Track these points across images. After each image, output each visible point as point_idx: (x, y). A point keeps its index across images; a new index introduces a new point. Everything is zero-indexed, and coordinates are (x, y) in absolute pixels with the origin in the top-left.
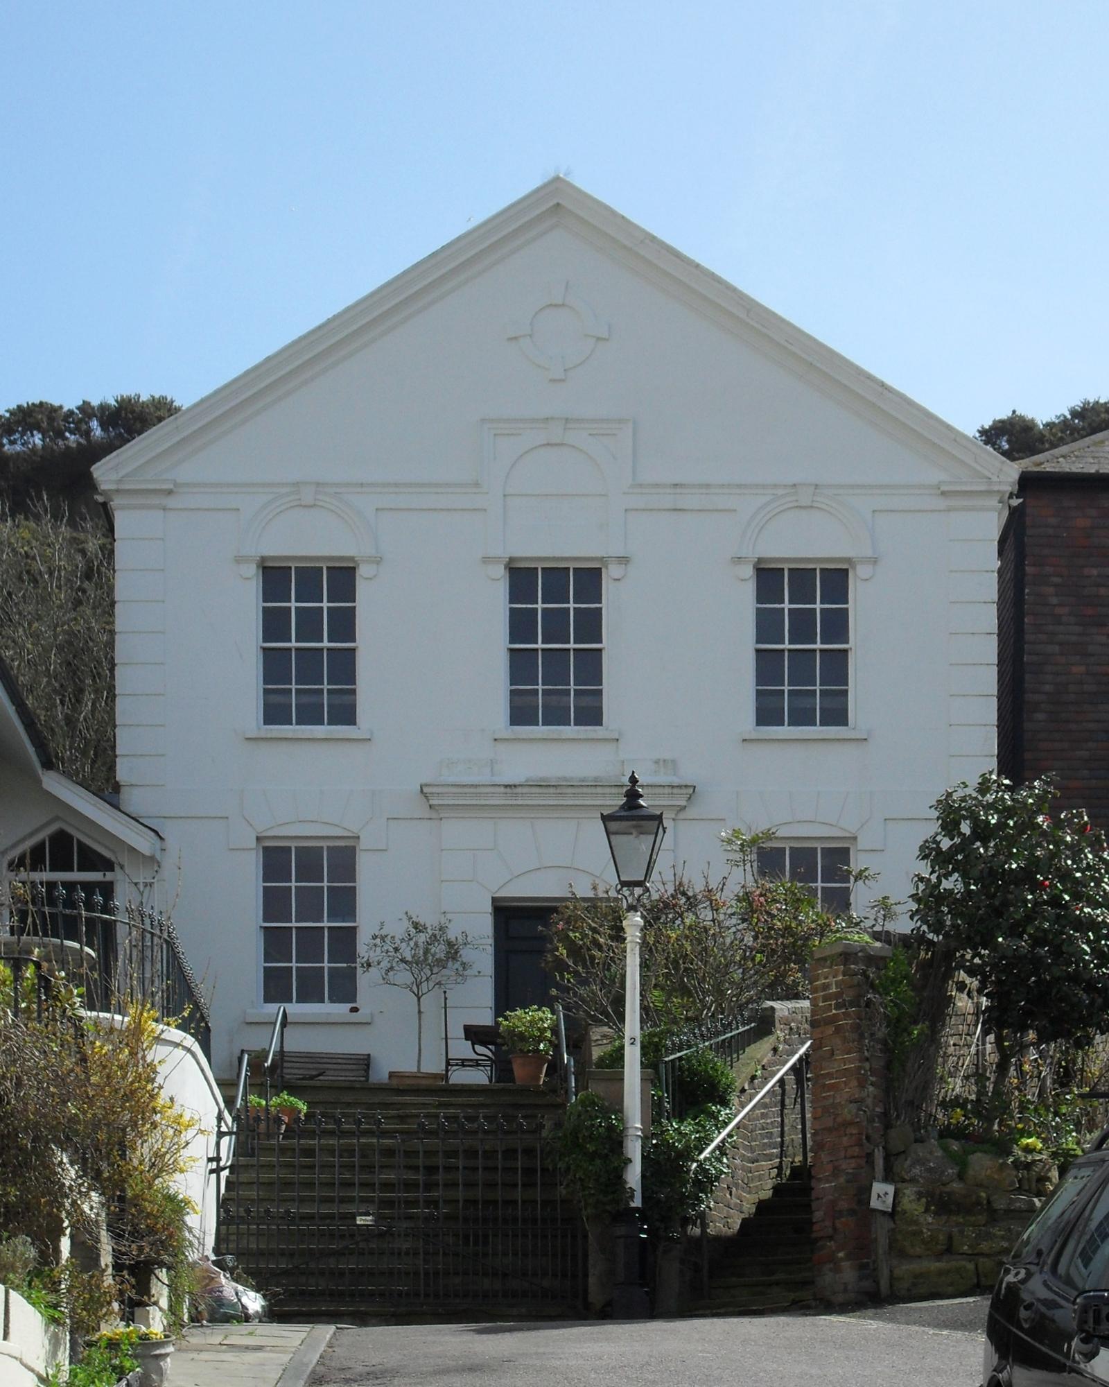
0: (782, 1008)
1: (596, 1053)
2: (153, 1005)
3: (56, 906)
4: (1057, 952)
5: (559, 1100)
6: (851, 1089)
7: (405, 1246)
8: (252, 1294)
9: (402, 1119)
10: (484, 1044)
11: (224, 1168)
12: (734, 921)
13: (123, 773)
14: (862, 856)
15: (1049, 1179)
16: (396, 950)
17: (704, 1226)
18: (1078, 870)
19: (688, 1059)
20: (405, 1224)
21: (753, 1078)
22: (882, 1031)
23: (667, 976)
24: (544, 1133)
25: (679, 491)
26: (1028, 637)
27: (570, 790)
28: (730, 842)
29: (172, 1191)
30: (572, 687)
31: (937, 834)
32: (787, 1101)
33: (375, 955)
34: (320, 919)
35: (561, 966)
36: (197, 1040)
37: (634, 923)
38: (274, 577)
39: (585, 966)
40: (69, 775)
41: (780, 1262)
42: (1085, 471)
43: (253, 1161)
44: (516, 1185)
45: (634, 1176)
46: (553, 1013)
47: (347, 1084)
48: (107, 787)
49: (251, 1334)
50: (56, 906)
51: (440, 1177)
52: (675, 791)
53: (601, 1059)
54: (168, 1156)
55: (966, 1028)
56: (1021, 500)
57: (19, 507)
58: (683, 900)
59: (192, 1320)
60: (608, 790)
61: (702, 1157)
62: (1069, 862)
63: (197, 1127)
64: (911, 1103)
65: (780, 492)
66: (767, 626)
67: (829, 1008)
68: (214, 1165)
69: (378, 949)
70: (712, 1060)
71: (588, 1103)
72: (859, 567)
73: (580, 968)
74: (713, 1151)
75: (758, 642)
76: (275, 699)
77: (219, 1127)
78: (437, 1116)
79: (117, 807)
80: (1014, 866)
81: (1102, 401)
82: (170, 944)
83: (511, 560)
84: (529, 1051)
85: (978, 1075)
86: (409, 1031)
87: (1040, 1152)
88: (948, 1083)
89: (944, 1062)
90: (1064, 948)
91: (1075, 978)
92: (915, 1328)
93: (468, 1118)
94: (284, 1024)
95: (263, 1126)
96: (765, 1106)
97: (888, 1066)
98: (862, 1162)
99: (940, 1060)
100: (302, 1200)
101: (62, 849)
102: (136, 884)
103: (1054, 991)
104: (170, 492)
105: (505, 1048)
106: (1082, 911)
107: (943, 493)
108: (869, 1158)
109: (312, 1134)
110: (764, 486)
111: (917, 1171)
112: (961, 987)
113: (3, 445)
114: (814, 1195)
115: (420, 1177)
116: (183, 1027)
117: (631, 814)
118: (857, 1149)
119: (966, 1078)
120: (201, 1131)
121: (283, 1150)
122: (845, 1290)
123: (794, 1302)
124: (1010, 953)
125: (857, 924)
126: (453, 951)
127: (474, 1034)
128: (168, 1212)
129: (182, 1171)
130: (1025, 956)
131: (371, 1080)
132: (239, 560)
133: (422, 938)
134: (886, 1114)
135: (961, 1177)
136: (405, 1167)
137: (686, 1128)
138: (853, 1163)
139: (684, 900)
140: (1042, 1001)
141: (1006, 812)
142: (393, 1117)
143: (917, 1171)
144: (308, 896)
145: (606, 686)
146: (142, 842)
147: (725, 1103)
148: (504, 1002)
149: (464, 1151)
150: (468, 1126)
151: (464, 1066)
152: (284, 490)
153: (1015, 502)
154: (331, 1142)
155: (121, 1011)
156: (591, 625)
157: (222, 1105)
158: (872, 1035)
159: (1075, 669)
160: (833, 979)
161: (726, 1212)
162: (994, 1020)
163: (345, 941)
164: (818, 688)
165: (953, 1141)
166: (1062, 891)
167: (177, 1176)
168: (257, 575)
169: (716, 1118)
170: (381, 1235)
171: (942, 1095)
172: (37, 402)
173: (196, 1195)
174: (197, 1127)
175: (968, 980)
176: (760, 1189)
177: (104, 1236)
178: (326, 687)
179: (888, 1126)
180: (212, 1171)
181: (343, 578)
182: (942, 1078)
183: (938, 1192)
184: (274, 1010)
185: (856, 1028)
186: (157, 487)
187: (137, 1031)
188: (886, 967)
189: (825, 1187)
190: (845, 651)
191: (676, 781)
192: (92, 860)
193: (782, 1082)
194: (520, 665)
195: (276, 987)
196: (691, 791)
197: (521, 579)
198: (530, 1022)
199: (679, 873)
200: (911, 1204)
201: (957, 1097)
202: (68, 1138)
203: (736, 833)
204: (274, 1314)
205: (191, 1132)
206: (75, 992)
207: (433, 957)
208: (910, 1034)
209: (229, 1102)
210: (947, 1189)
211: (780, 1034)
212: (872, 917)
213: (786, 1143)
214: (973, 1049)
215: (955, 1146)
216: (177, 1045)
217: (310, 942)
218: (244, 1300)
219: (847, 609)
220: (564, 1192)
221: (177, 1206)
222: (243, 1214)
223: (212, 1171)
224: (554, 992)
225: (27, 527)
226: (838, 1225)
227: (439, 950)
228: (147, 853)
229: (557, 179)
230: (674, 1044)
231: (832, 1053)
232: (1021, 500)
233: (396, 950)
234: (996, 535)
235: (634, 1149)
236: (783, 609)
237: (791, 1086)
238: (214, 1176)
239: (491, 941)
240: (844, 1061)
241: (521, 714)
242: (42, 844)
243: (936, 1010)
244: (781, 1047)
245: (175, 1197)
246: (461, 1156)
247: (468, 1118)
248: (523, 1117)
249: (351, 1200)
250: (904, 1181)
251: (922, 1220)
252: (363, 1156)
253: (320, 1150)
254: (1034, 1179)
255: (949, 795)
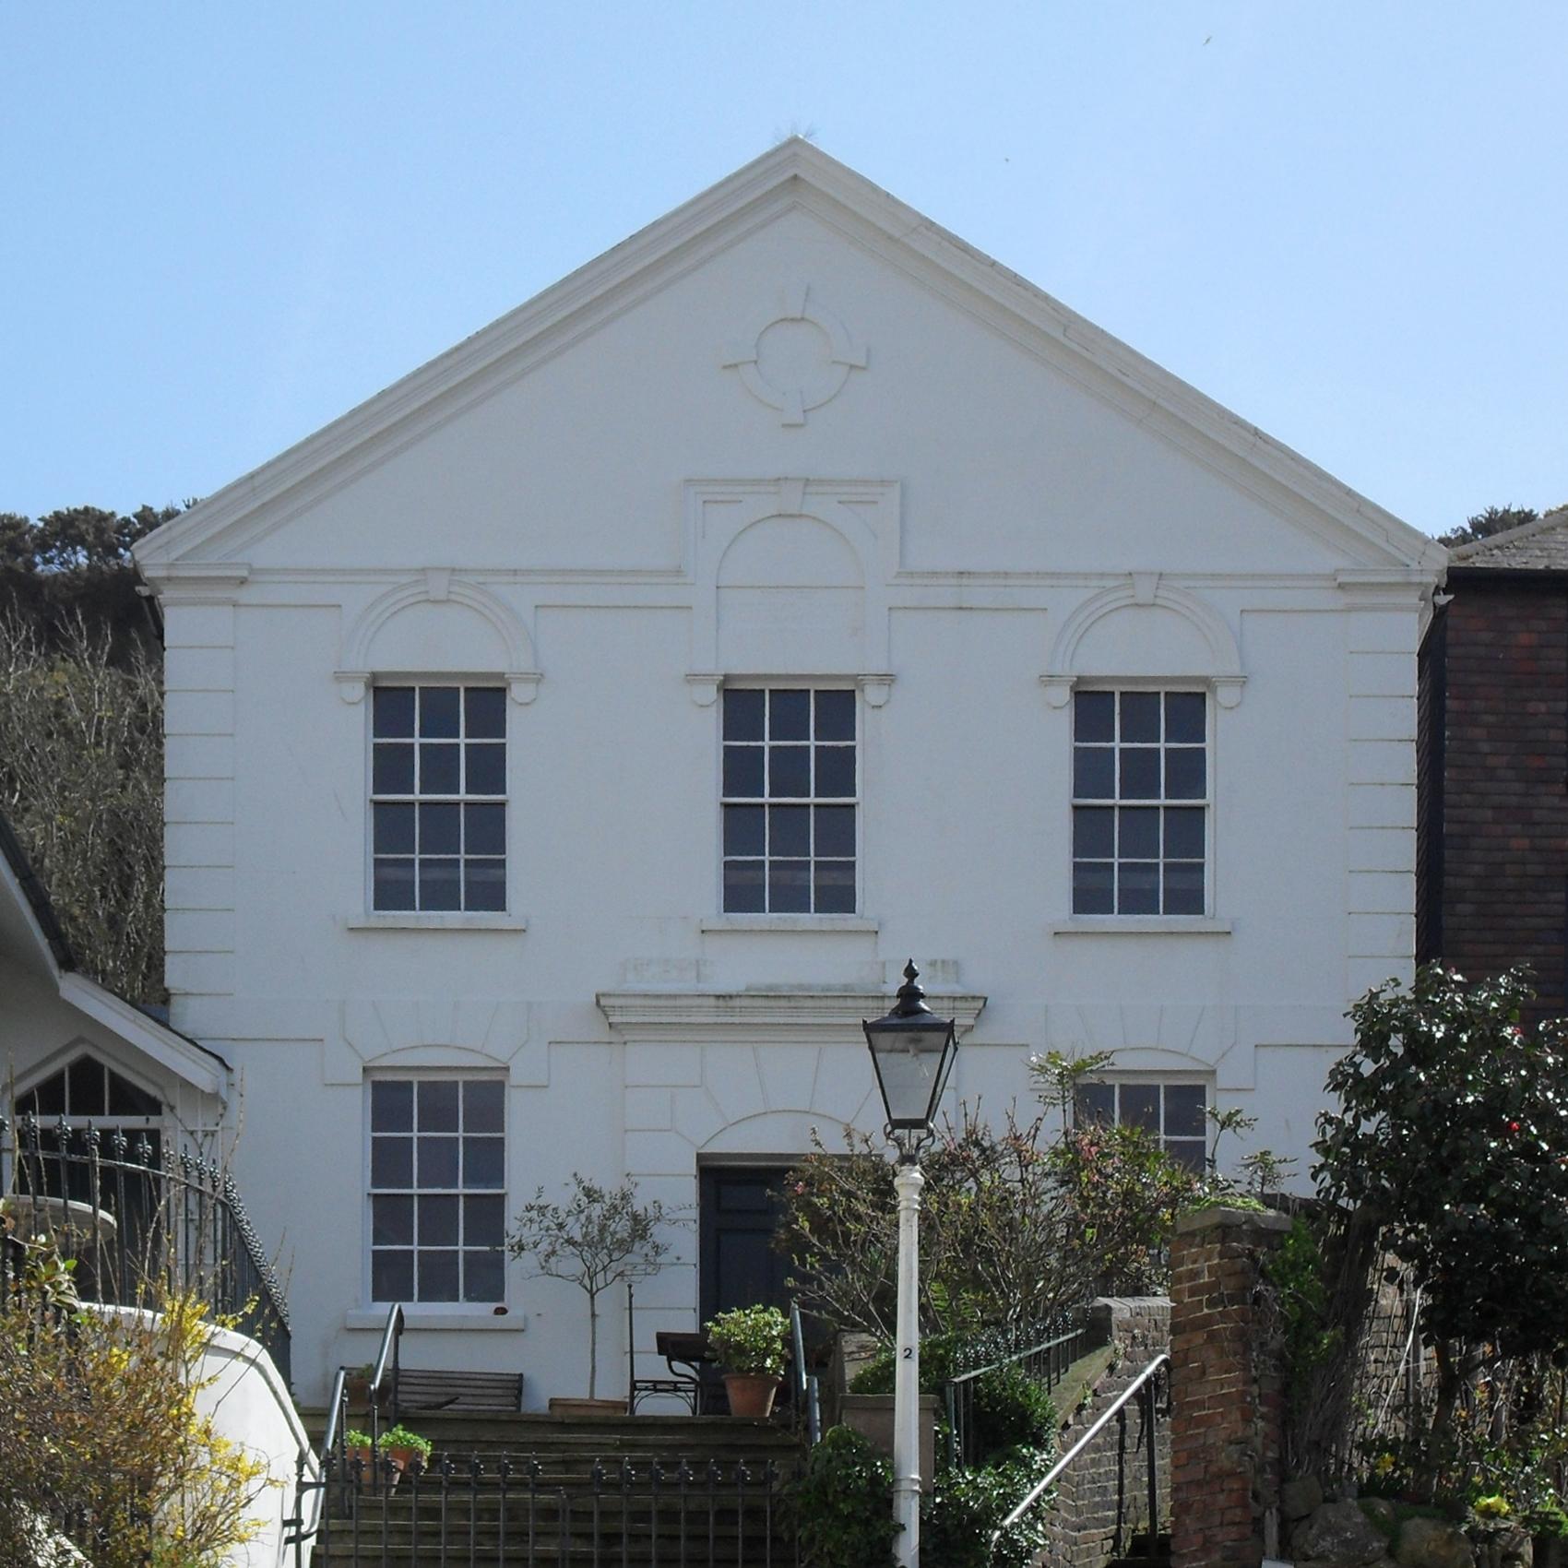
0: (1121, 1307)
1: (851, 1372)
2: (201, 1297)
3: (57, 1150)
4: (1533, 1223)
5: (796, 1440)
6: (1231, 1423)
9: (567, 1465)
10: (686, 1360)
13: (174, 976)
16: (561, 1226)
19: (987, 1379)
21: (1081, 1407)
22: (1277, 1340)
23: (954, 1261)
24: (776, 1486)
25: (965, 581)
27: (809, 1003)
28: (1042, 1070)
30: (812, 858)
32: (1128, 1442)
33: (530, 1234)
36: (265, 1346)
37: (910, 1182)
39: (835, 1245)
42: (1530, 566)
43: (350, 1525)
44: (678, 1537)
46: (785, 1315)
47: (488, 1416)
48: (154, 1001)
50: (57, 1150)
52: (958, 1004)
53: (860, 1380)
54: (221, 1518)
55: (1392, 1337)
56: (1451, 597)
57: (51, 639)
58: (972, 1155)
60: (862, 1003)
61: (1007, 1522)
62: (1550, 1095)
63: (264, 1475)
65: (1111, 583)
66: (1089, 773)
68: (293, 1531)
69: (535, 1227)
73: (829, 1249)
74: (1024, 1513)
75: (1076, 795)
76: (391, 873)
78: (619, 1462)
79: (165, 1025)
80: (1470, 1099)
82: (228, 1207)
83: (727, 678)
84: (750, 1370)
85: (1408, 1405)
87: (1506, 1517)
88: (1367, 1417)
89: (1362, 1386)
90: (1544, 1220)
93: (663, 1464)
94: (399, 1330)
95: (366, 1473)
96: (1097, 1448)
97: (1285, 1390)
99: (1356, 1383)
101: (88, 1084)
102: (192, 1133)
103: (1529, 1283)
107: (1341, 586)
108: (1258, 1523)
109: (434, 1486)
110: (1086, 576)
111: (1327, 1543)
112: (1392, 1275)
113: (36, 565)
116: (245, 1328)
117: (908, 1022)
118: (1238, 1511)
119: (1395, 1410)
121: (394, 1510)
124: (1463, 1226)
126: (640, 1227)
127: (670, 1346)
129: (241, 1541)
130: (1487, 1230)
131: (523, 1410)
132: (340, 677)
133: (597, 1210)
134: (1281, 1461)
136: (572, 1534)
138: (1234, 1532)
139: (975, 1153)
141: (1458, 1022)
142: (555, 1463)
143: (1327, 1543)
144: (437, 1165)
146: (201, 1073)
147: (1040, 1444)
149: (660, 1512)
151: (656, 1391)
152: (405, 579)
153: (1443, 599)
154: (466, 1497)
155: (151, 1302)
156: (839, 771)
157: (306, 1443)
158: (1262, 1345)
159: (1514, 843)
160: (1204, 1263)
162: (1437, 1327)
163: (488, 1215)
164: (1161, 861)
169: (1028, 1466)
171: (1359, 1432)
172: (80, 507)
174: (264, 1475)
179: (1284, 1478)
180: (289, 1540)
181: (488, 703)
182: (1357, 1409)
184: (386, 1311)
185: (1240, 1335)
186: (228, 573)
187: (177, 1334)
188: (1282, 1246)
190: (1201, 809)
192: (130, 1099)
193: (1120, 1414)
195: (390, 1278)
196: (981, 1004)
197: (740, 705)
198: (753, 1327)
199: (972, 1115)
201: (1382, 1437)
202: (48, 1493)
203: (1053, 1057)
205: (255, 1484)
206: (62, 1266)
207: (614, 1236)
208: (1318, 1343)
209: (317, 1440)
211: (1121, 1346)
213: (1126, 1502)
214: (1402, 1367)
215: (1383, 1508)
217: (438, 1214)
219: (1203, 750)
223: (289, 1540)
224: (790, 1282)
227: (621, 1227)
228: (208, 1089)
229: (794, 141)
230: (966, 1357)
232: (1451, 597)
234: (1416, 647)
235: (909, 1512)
236: (1113, 749)
237: (1134, 1421)
238: (292, 1546)
239: (694, 1214)
241: (740, 895)
242: (59, 1077)
243: (1352, 1307)
244: (1120, 1364)
246: (654, 1521)
247: (663, 1464)
248: (746, 1463)
253: (449, 1509)
254: (1500, 1555)
255: (1374, 996)
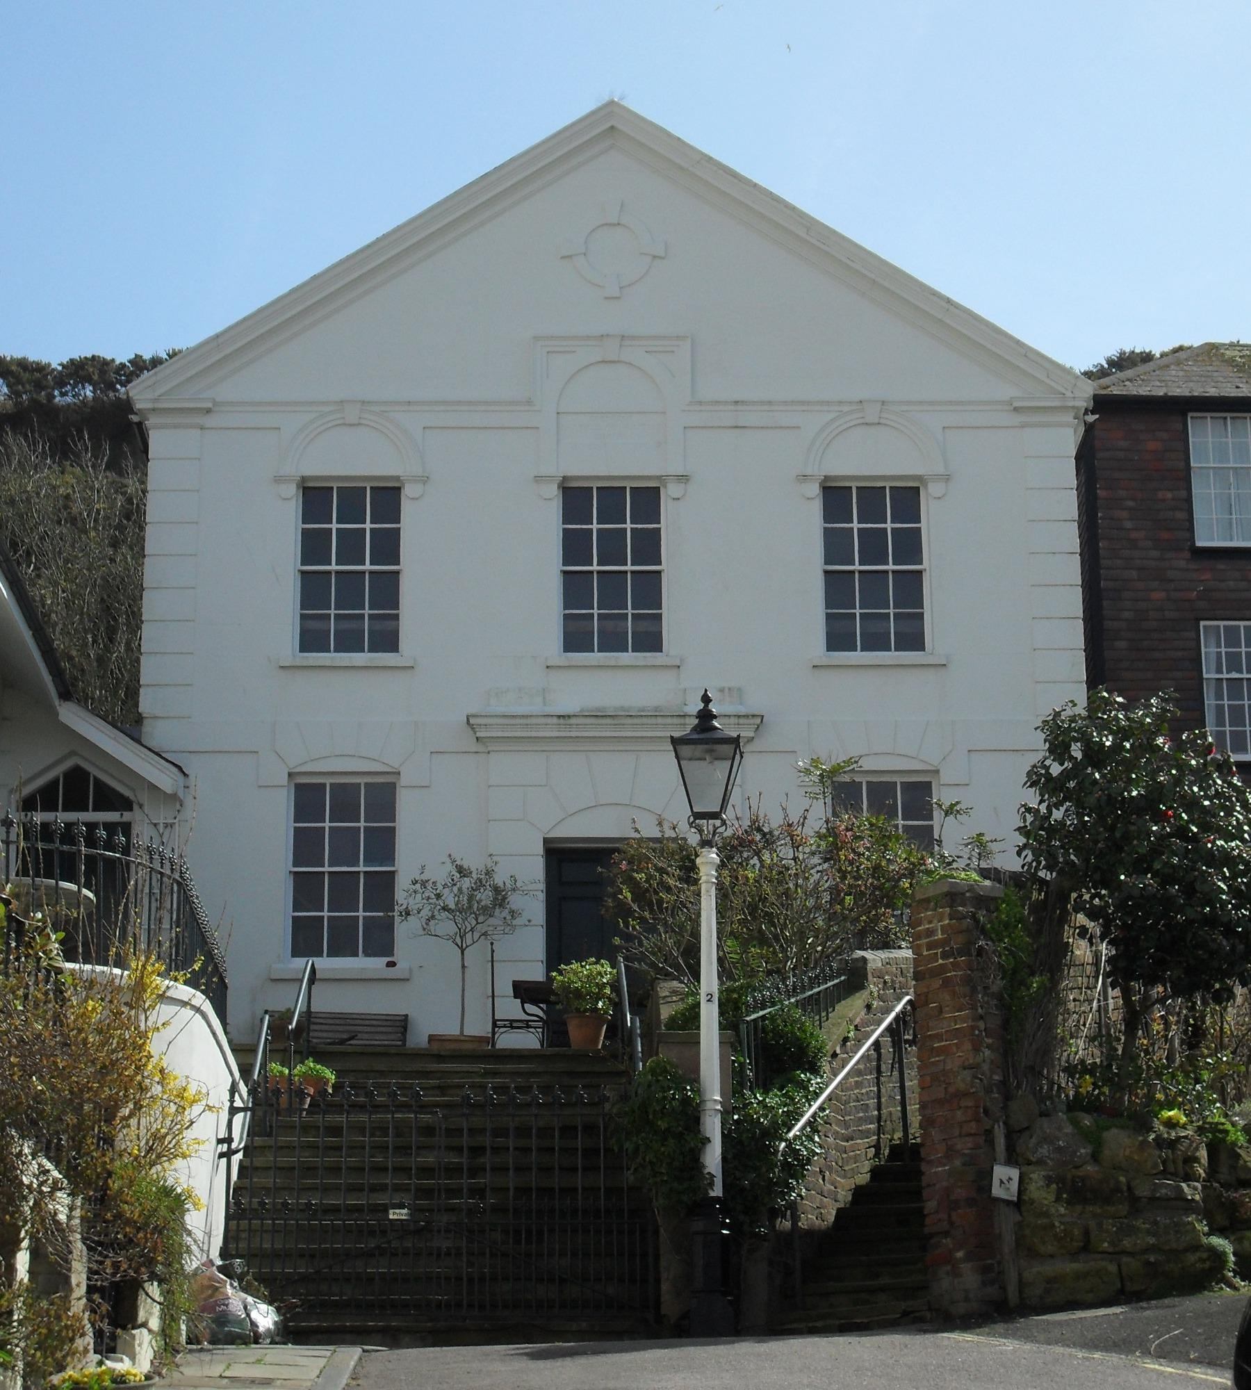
0: (876, 958)
1: (666, 1012)
2: (159, 958)
4: (1189, 890)
7: (446, 1245)
8: (264, 1307)
9: (442, 1089)
11: (237, 1151)
12: (816, 860)
14: (944, 790)
15: (1197, 1160)
16: (438, 896)
17: (795, 1219)
18: (1206, 797)
19: (772, 1017)
20: (445, 1218)
21: (846, 1040)
22: (997, 984)
25: (740, 407)
26: (1104, 562)
27: (629, 721)
28: (807, 772)
29: (170, 1182)
30: (630, 611)
31: (1046, 758)
32: (883, 1067)
33: (415, 903)
34: (356, 864)
35: (625, 912)
36: (208, 997)
38: (315, 498)
39: (652, 911)
40: (95, 712)
41: (883, 1263)
45: (713, 1158)
46: (612, 967)
48: (130, 722)
49: (259, 1361)
51: (487, 1160)
52: (741, 721)
53: (672, 1019)
54: (169, 1138)
55: (1085, 980)
58: (752, 840)
59: (189, 1342)
60: (669, 721)
61: (791, 1135)
62: (1195, 789)
63: (204, 1103)
64: (1032, 1068)
65: (846, 408)
66: (835, 547)
67: (934, 958)
69: (419, 896)
70: (799, 1019)
71: (659, 1071)
72: (930, 486)
73: (647, 914)
74: (804, 1128)
76: (312, 625)
77: (232, 1101)
80: (1134, 793)
81: (1138, 351)
82: (182, 886)
83: (565, 478)
84: (586, 1010)
85: (1101, 1036)
86: (452, 988)
87: (1184, 1127)
89: (1065, 1020)
90: (1198, 886)
91: (1212, 921)
92: (1059, 1350)
94: (312, 980)
95: (284, 1098)
97: (1006, 1024)
98: (981, 1140)
99: (1060, 1017)
100: (326, 1189)
101: (79, 786)
102: (155, 825)
103: (1189, 936)
104: (208, 411)
105: (559, 1007)
106: (1213, 843)
107: (1016, 409)
109: (337, 1108)
110: (828, 403)
111: (1044, 1150)
112: (1083, 932)
113: (54, 397)
114: (925, 1180)
115: (464, 1160)
118: (973, 1124)
120: (210, 1108)
121: (306, 1129)
122: (967, 1299)
123: (905, 1314)
125: (949, 864)
126: (500, 897)
127: (524, 991)
128: (163, 1211)
129: (184, 1156)
130: (1154, 895)
132: (278, 480)
133: (466, 883)
134: (1004, 1083)
135: (1095, 1157)
137: (771, 1101)
140: (1172, 948)
142: (433, 1088)
143: (1044, 1150)
144: (343, 846)
145: (665, 611)
146: (164, 779)
147: (815, 1070)
148: (557, 954)
150: (520, 1098)
151: (512, 1027)
153: (1091, 418)
155: (120, 963)
156: (649, 546)
158: (986, 988)
160: (938, 923)
161: (819, 1201)
162: (1121, 971)
163: (382, 887)
164: (891, 611)
165: (1084, 1114)
166: (1187, 822)
167: (179, 1163)
168: (297, 495)
169: (806, 1088)
170: (419, 1232)
171: (1064, 1059)
172: (89, 356)
173: (202, 1183)
174: (204, 1103)
175: (1090, 925)
176: (855, 1172)
177: (79, 1247)
178: (367, 612)
179: (1008, 1097)
180: (221, 1155)
181: (388, 498)
182: (1062, 1039)
183: (1069, 1176)
185: (967, 981)
186: (199, 405)
187: (139, 987)
188: (997, 909)
189: (937, 1172)
190: (920, 572)
191: (742, 710)
192: (109, 799)
193: (877, 1044)
194: (575, 589)
196: (759, 721)
197: (575, 498)
198: (588, 977)
199: (754, 808)
200: (1041, 1193)
203: (815, 762)
204: (289, 1333)
205: (197, 1109)
206: (53, 937)
207: (477, 904)
209: (245, 1071)
210: (1080, 1173)
211: (875, 989)
212: (966, 856)
213: (884, 1118)
215: (1087, 1121)
216: (184, 1004)
218: (254, 1315)
220: (632, 1178)
221: (176, 1202)
222: (255, 1206)
223: (221, 1155)
224: (617, 941)
225: (73, 473)
226: (954, 1218)
227: (485, 896)
228: (169, 791)
229: (611, 103)
231: (940, 1010)
233: (438, 896)
235: (713, 1127)
237: (887, 1050)
239: (542, 886)
240: (955, 1019)
241: (575, 639)
242: (55, 782)
244: (875, 1003)
245: (173, 1189)
249: (383, 1188)
250: (1029, 1163)
251: (1053, 1210)
252: (398, 1135)
255: (1057, 714)
